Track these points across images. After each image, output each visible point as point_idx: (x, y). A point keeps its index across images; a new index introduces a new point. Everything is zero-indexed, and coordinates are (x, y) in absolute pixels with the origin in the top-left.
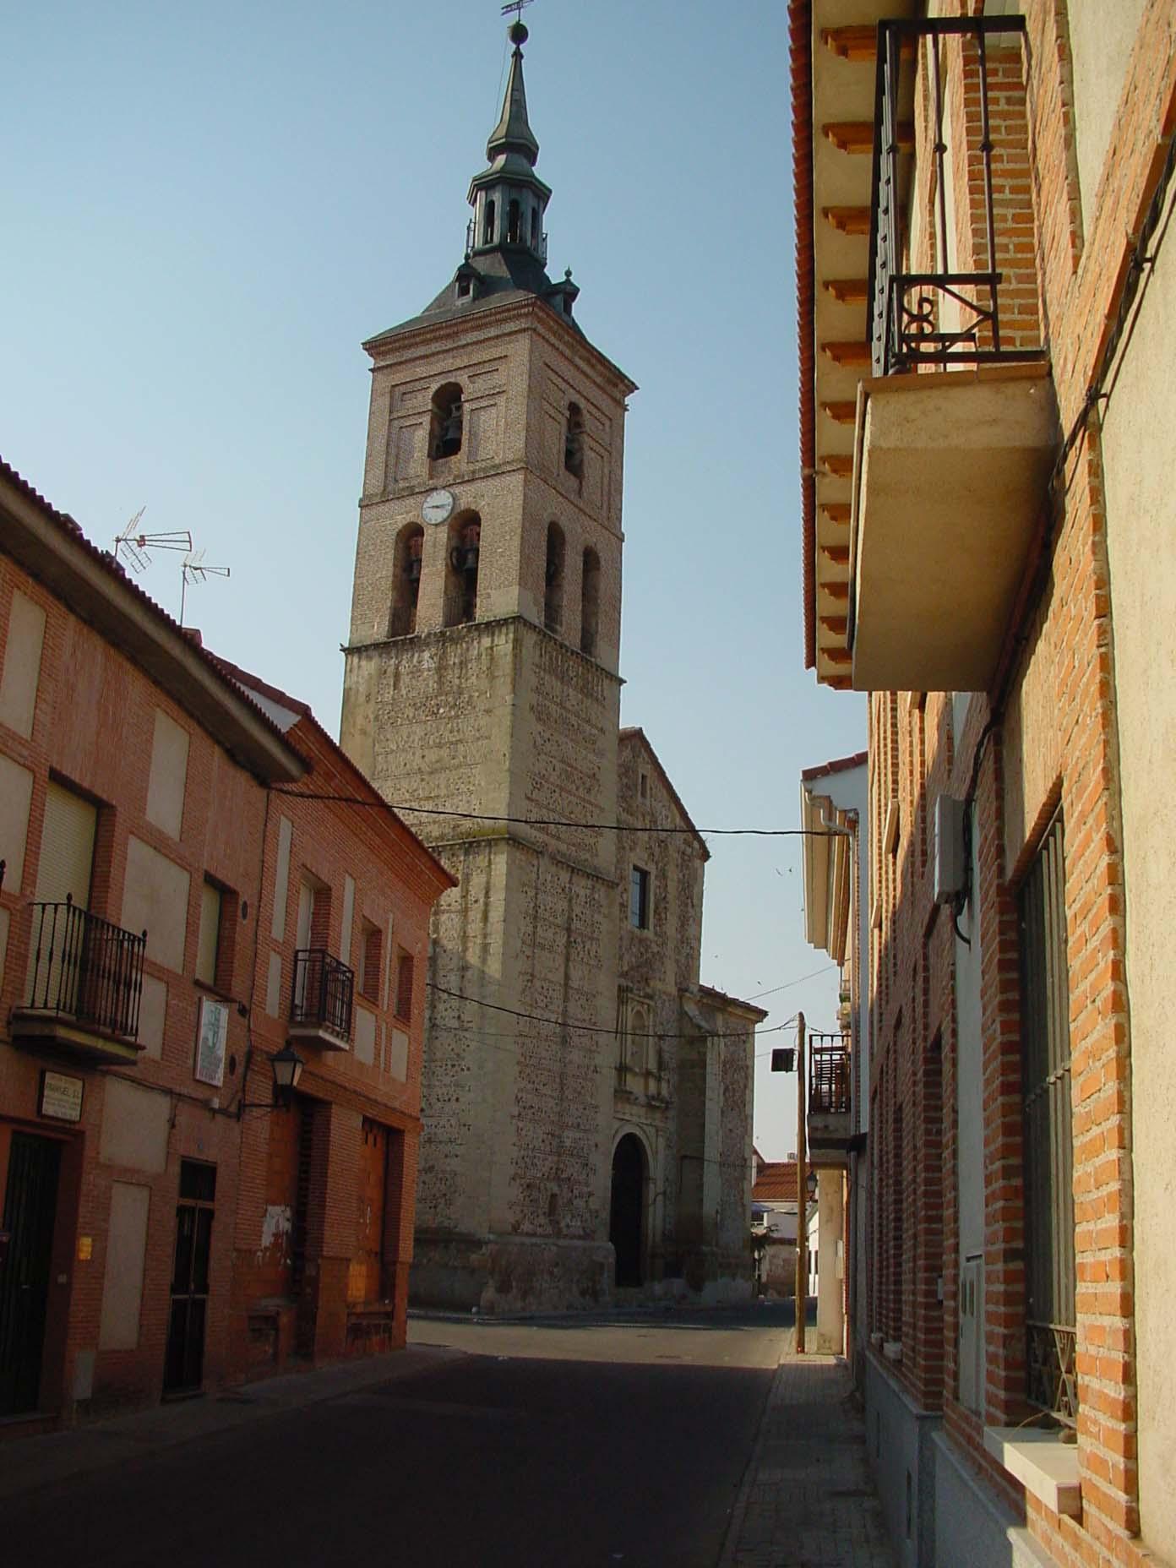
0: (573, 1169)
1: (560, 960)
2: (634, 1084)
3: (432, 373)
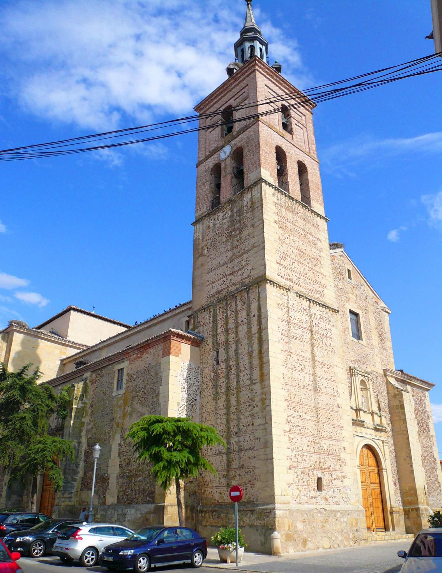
0: (330, 462)
1: (308, 346)
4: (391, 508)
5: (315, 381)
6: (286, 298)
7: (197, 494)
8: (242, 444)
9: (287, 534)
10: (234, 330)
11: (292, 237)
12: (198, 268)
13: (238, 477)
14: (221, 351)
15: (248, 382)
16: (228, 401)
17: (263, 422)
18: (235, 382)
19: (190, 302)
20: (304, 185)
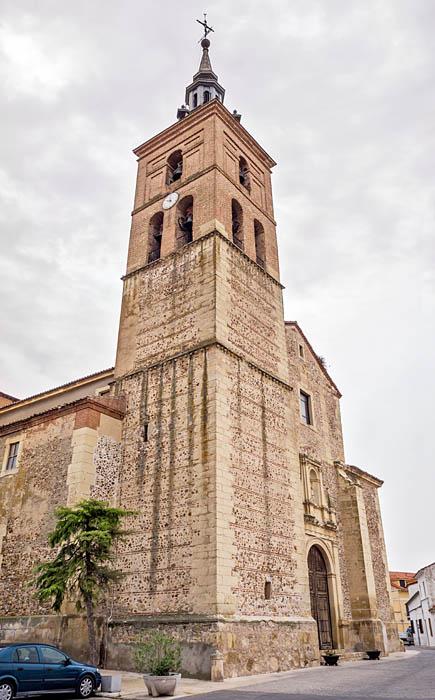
0: (280, 564)
2: (315, 513)
3: (165, 151)
4: (340, 621)
5: (265, 467)
6: (237, 367)
7: (107, 603)
8: (173, 538)
9: (229, 653)
10: (170, 401)
11: (245, 300)
12: (126, 329)
13: (166, 580)
14: (152, 425)
15: (187, 463)
16: (157, 485)
17: (205, 511)
18: (168, 463)
19: (113, 369)
20: (259, 246)
